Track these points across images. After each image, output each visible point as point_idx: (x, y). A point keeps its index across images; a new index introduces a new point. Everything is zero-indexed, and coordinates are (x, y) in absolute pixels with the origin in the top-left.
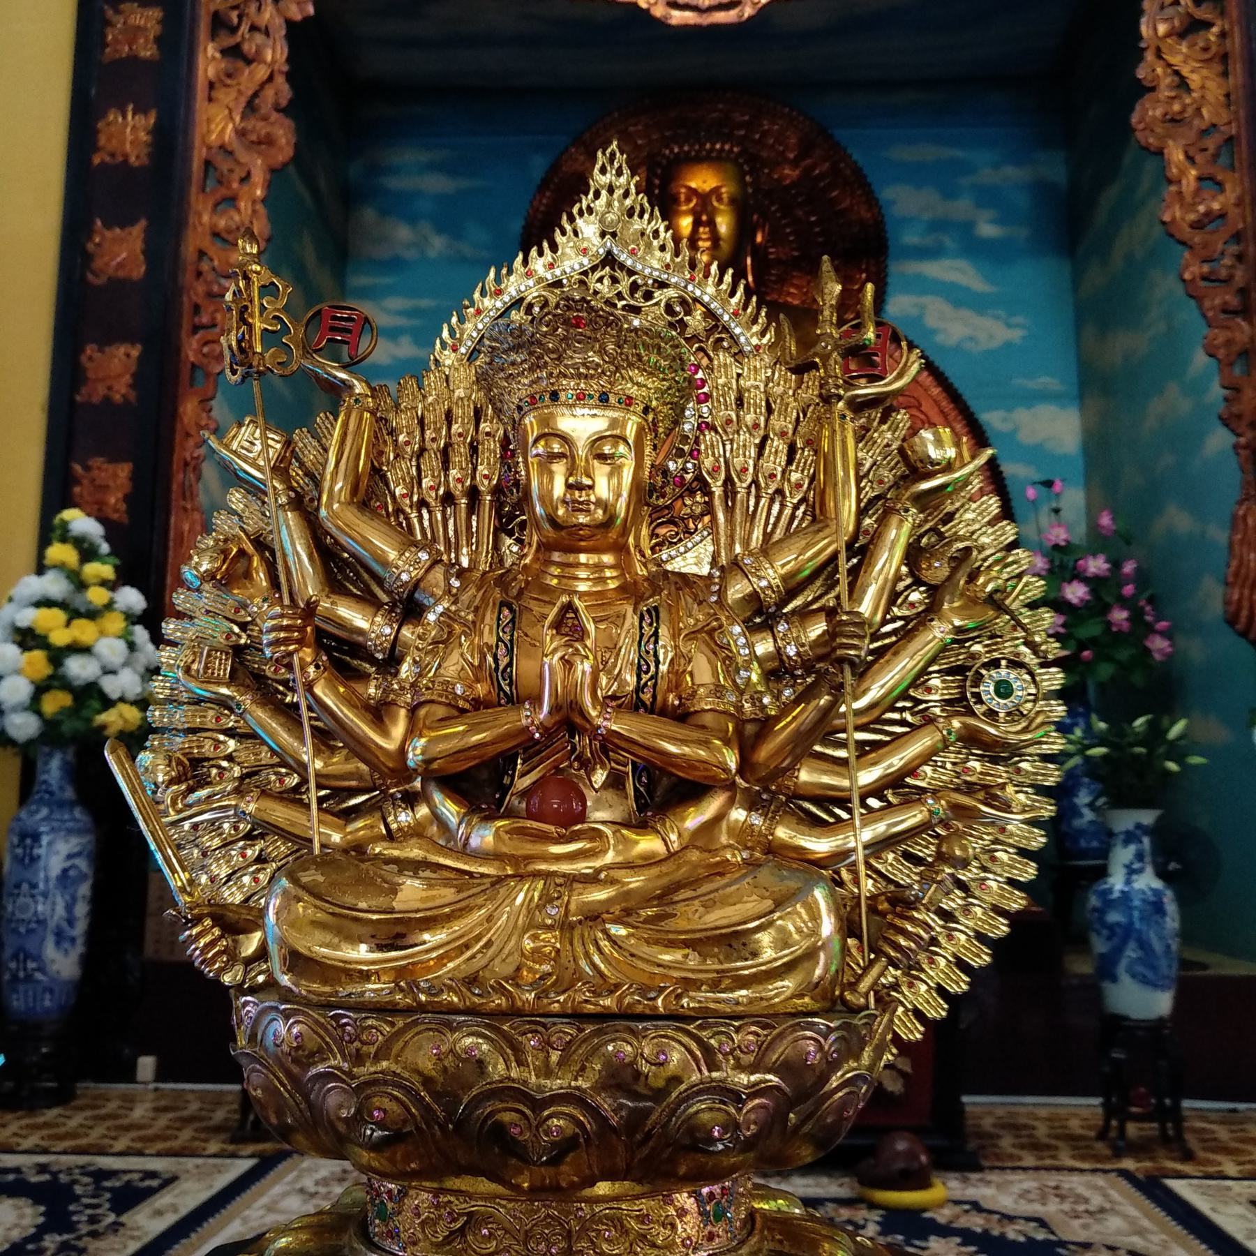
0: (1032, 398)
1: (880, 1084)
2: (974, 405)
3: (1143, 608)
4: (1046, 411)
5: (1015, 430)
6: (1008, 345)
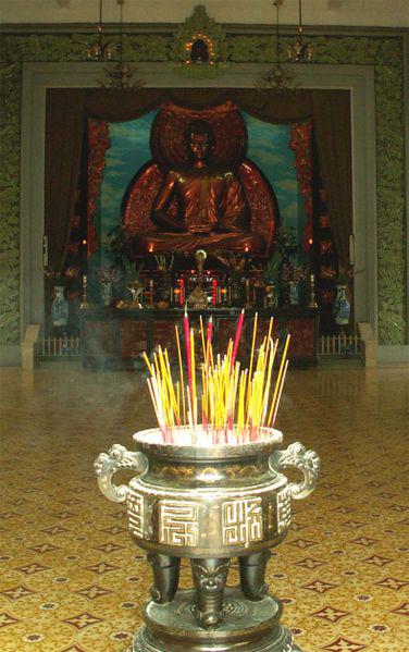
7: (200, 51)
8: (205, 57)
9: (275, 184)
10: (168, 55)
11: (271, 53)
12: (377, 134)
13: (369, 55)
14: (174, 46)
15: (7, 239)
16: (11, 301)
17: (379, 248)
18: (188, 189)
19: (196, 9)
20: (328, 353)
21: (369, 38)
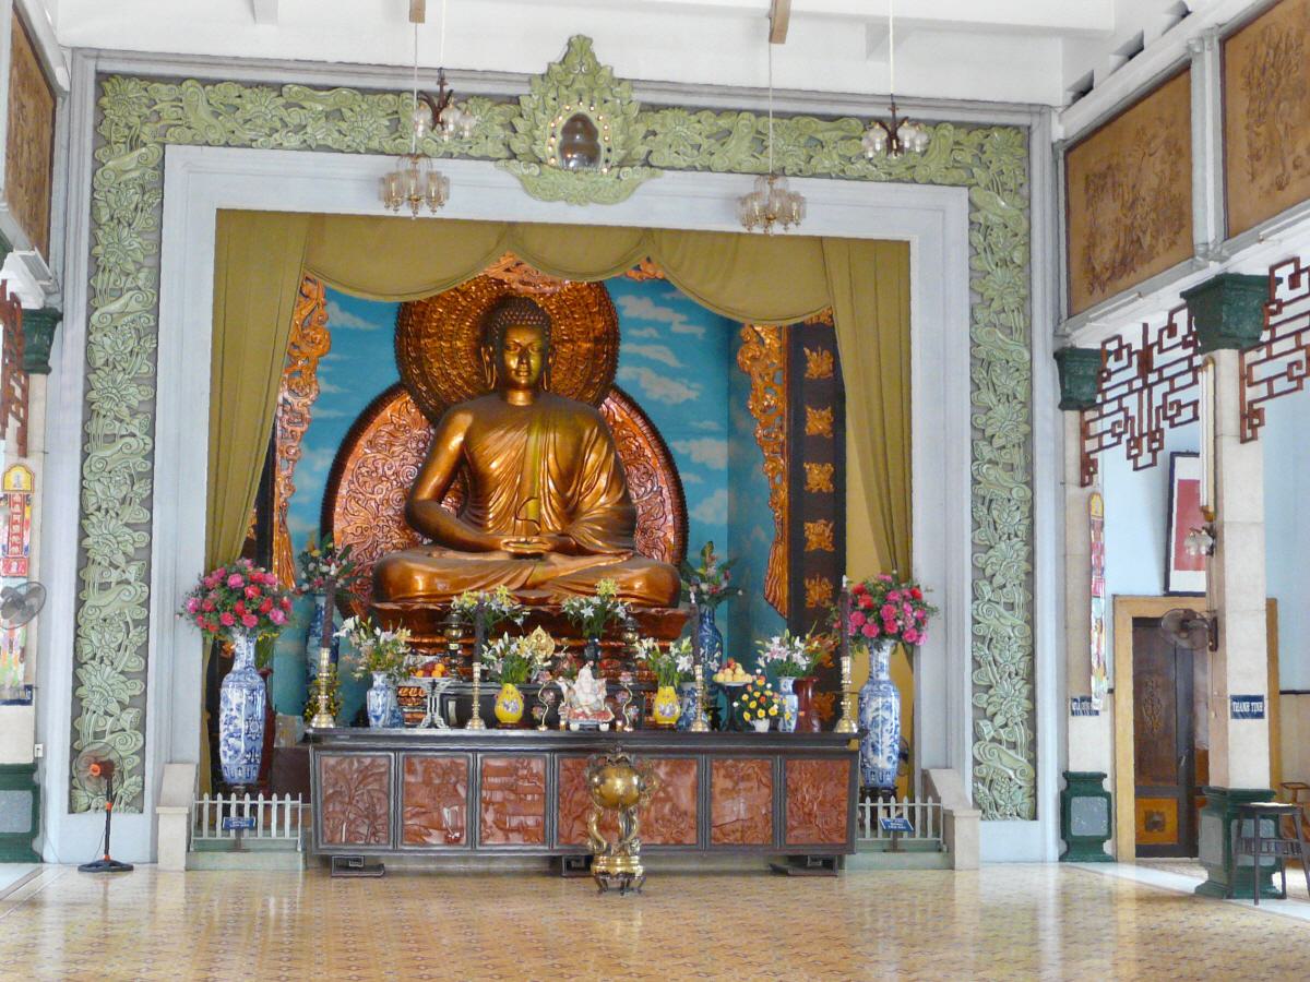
0: (701, 434)
1: (1062, 858)
2: (666, 437)
3: (828, 609)
4: (708, 442)
5: (690, 454)
6: (688, 401)
7: (581, 139)
8: (591, 155)
9: (677, 447)
10: (508, 147)
11: (739, 149)
12: (974, 344)
13: (957, 165)
14: (519, 124)
15: (120, 559)
16: (123, 707)
17: (975, 598)
18: (497, 455)
19: (570, 44)
20: (930, 837)
21: (958, 125)
